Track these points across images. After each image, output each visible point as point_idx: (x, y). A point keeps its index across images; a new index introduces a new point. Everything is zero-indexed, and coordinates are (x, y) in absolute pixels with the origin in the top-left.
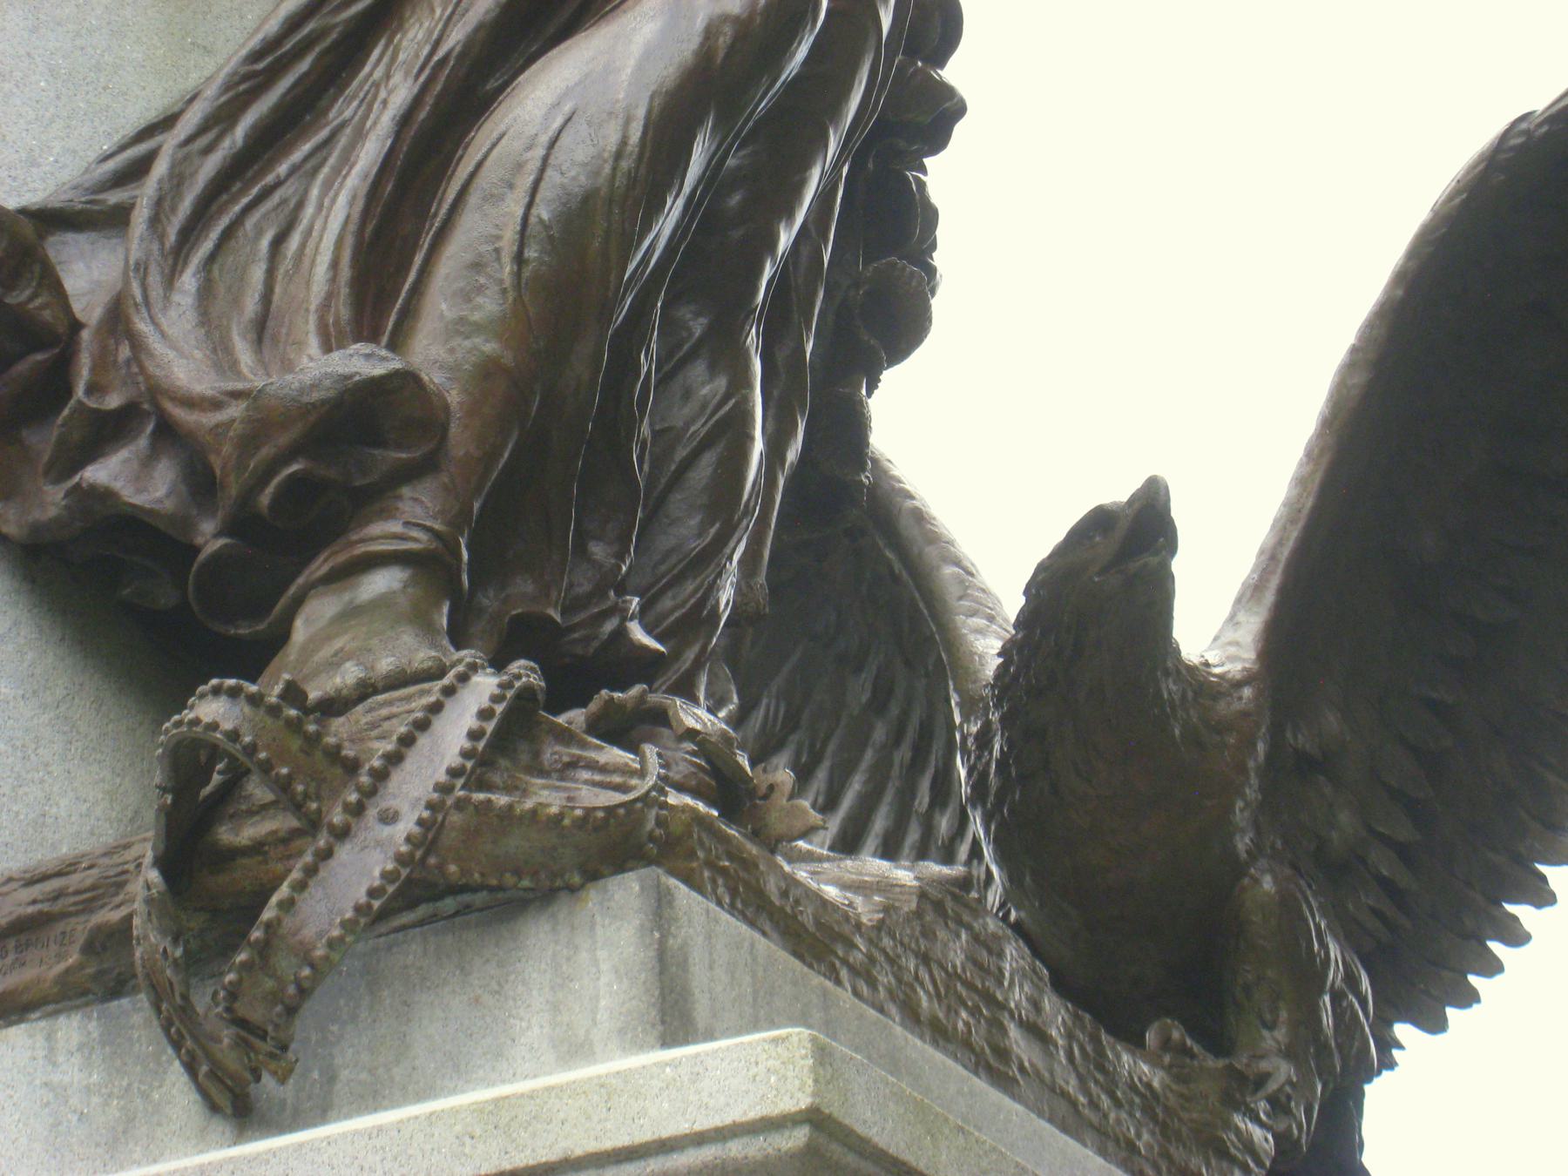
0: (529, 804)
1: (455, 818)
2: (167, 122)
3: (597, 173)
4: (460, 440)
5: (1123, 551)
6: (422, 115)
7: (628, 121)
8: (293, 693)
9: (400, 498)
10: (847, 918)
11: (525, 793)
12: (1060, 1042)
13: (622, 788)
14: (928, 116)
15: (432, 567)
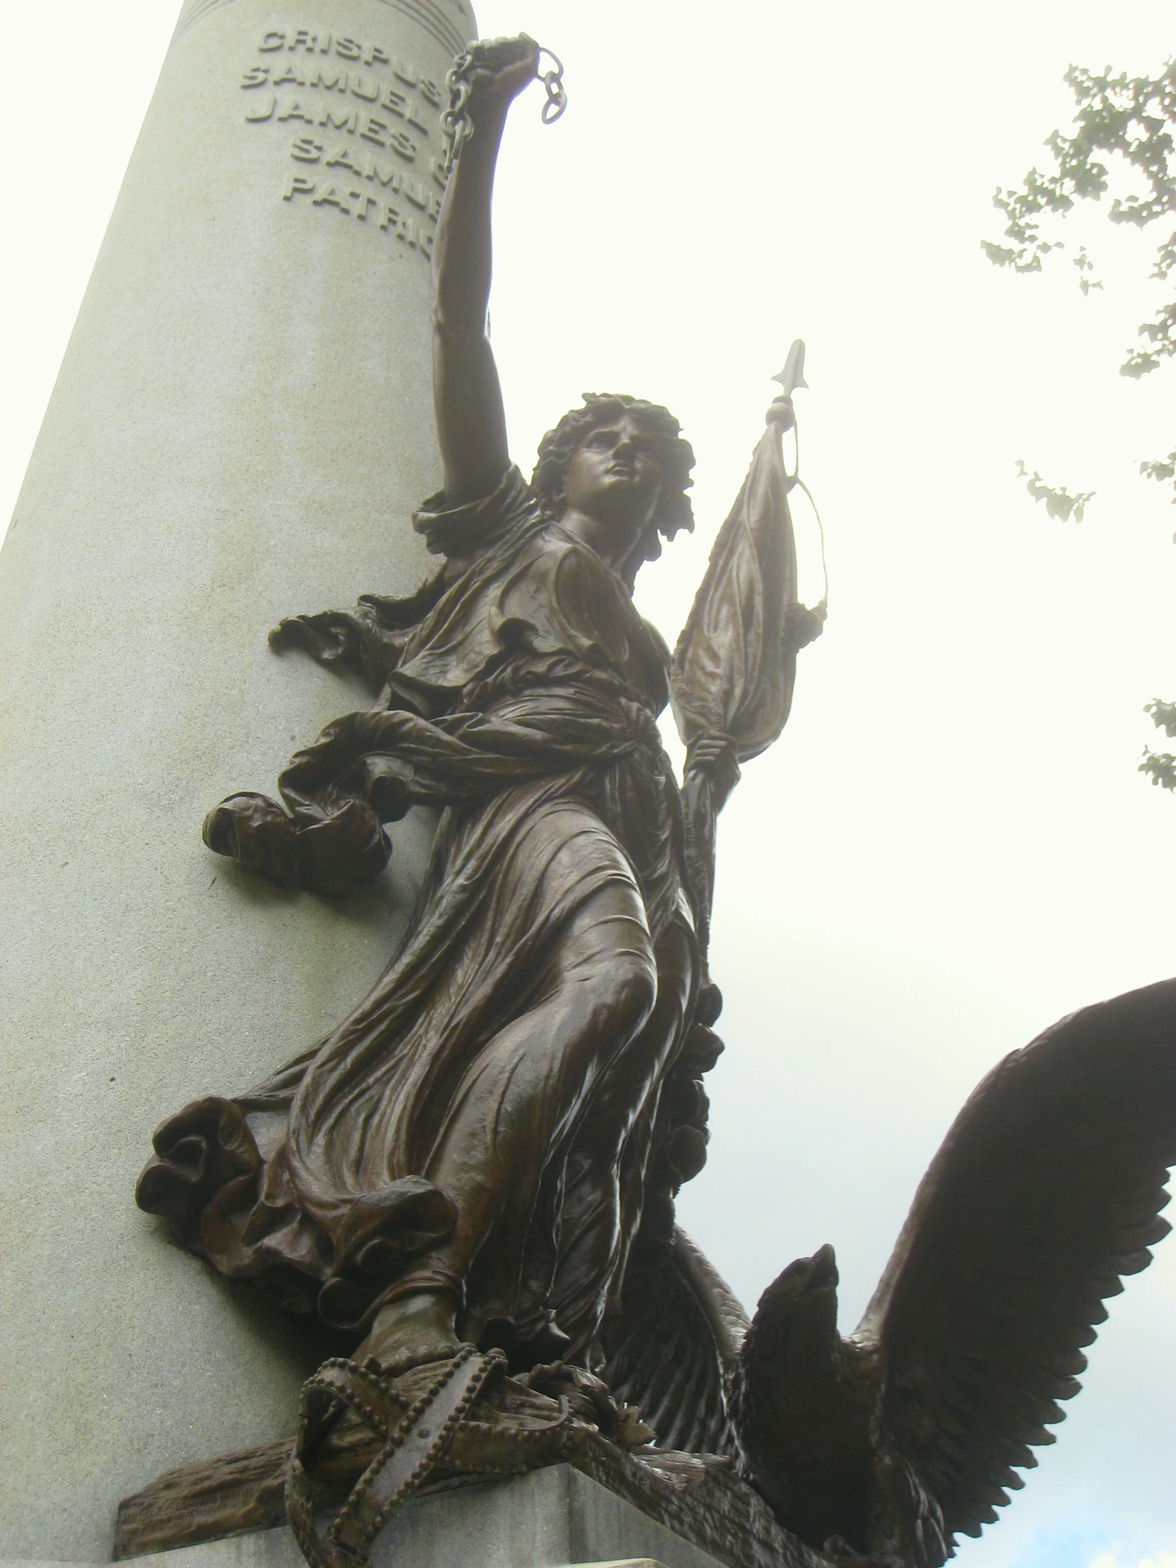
0: (499, 1428)
1: (460, 1435)
2: (311, 1055)
3: (536, 1087)
4: (463, 1227)
5: (812, 1280)
6: (445, 1054)
7: (553, 1059)
8: (373, 1365)
9: (431, 1258)
10: (667, 1487)
11: (497, 1421)
12: (780, 1550)
13: (549, 1418)
14: (706, 1051)
15: (445, 1295)
